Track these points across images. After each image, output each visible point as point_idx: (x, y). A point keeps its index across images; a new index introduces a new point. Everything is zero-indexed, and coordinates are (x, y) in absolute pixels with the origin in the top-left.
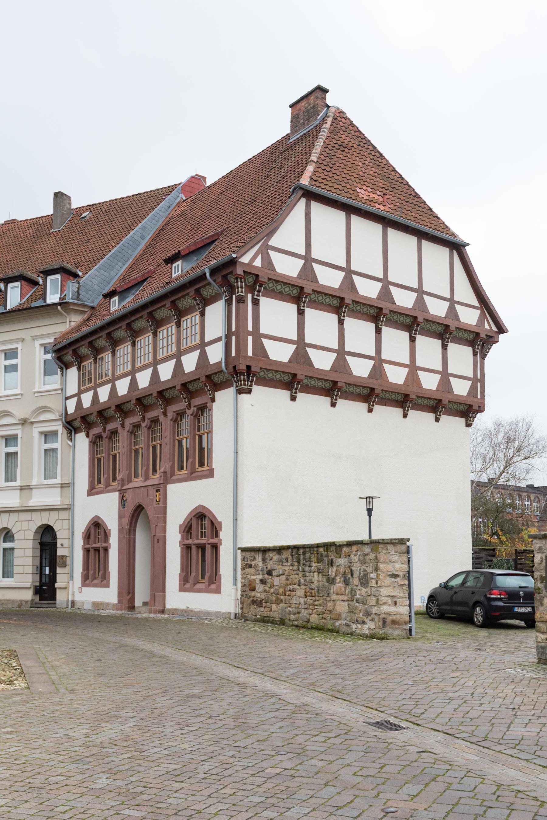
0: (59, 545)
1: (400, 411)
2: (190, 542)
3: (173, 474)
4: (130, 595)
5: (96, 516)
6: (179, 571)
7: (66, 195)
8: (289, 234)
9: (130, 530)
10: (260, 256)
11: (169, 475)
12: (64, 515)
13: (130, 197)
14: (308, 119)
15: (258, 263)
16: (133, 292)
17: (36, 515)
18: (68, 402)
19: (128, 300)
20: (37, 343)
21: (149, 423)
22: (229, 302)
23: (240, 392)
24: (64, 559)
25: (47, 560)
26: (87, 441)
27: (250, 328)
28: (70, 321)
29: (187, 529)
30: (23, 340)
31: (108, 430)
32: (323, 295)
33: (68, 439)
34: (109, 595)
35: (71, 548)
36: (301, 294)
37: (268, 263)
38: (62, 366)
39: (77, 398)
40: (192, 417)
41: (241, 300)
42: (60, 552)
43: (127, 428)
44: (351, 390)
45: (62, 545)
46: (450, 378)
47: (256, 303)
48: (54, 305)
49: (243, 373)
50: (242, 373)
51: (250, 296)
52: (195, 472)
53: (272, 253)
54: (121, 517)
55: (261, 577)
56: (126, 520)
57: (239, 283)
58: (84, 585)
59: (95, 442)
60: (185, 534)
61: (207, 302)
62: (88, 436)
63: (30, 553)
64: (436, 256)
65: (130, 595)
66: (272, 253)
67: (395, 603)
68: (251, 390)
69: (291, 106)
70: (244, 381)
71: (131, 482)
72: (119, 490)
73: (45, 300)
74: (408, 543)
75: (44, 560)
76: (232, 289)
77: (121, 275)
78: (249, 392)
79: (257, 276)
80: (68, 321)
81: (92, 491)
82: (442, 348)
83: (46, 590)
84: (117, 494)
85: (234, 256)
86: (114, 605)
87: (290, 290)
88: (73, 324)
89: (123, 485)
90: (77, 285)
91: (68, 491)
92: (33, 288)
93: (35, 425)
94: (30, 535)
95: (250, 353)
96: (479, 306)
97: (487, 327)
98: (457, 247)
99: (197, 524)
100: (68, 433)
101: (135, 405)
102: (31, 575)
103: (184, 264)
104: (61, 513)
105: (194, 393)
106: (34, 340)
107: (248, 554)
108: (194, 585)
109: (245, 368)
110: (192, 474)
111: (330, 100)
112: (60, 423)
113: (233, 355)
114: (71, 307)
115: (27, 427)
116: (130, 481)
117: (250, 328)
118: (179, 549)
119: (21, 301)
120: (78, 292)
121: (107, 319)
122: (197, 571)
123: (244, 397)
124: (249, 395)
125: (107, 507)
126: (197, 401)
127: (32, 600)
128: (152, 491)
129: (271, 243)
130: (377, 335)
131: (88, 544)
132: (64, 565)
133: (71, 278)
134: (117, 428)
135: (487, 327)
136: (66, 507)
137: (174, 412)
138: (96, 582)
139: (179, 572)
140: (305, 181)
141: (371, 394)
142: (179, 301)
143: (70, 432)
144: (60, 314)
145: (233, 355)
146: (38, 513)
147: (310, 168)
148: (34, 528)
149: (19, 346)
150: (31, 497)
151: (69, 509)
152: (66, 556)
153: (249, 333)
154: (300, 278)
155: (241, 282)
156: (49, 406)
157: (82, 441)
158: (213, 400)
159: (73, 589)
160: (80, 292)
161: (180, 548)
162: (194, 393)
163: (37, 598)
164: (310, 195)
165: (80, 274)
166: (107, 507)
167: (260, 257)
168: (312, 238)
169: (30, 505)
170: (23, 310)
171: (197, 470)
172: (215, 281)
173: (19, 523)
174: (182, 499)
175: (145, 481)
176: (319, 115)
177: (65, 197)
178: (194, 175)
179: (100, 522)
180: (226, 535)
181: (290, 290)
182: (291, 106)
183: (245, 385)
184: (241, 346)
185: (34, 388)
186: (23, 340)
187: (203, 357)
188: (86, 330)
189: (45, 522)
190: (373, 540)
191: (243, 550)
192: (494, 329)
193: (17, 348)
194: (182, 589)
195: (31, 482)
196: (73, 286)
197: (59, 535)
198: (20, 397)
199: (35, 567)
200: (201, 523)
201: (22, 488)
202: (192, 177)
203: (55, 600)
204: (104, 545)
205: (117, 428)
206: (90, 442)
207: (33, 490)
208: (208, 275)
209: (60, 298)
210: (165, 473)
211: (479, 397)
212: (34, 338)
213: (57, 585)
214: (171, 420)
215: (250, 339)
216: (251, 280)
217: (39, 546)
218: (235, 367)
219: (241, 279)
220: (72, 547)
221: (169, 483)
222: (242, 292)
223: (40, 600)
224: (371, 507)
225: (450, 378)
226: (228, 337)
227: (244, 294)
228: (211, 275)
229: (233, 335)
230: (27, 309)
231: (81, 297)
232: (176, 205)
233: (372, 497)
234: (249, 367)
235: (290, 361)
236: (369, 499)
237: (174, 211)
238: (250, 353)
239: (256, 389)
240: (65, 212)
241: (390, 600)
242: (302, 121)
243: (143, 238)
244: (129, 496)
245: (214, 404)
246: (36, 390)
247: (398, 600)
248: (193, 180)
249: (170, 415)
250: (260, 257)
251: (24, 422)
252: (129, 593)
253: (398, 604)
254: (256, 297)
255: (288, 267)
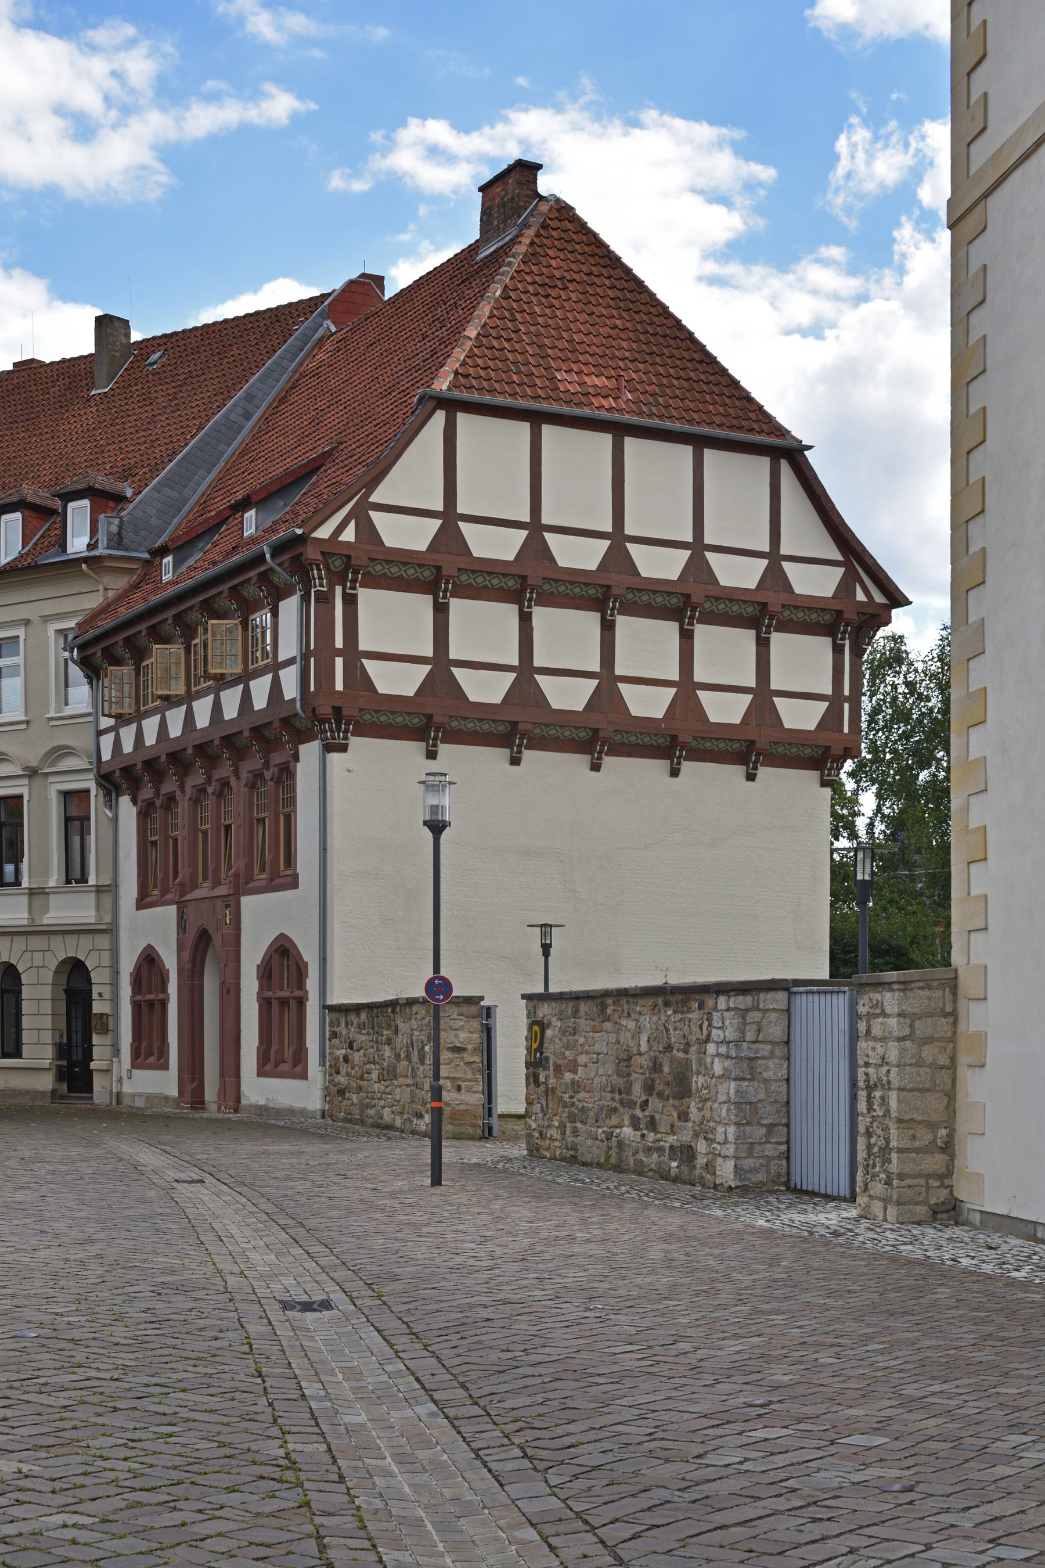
0: (95, 996)
1: (664, 765)
2: (269, 994)
3: (250, 878)
4: (196, 1083)
5: (282, 934)
6: (256, 1043)
7: (119, 318)
8: (414, 477)
9: (193, 971)
10: (353, 523)
11: (242, 880)
12: (103, 942)
13: (240, 318)
14: (505, 221)
15: (349, 535)
16: (200, 546)
17: (56, 942)
18: (103, 738)
19: (191, 562)
20: (53, 627)
21: (218, 788)
22: (305, 599)
23: (328, 748)
24: (104, 1019)
25: (79, 1020)
26: (134, 810)
27: (339, 643)
28: (106, 589)
29: (266, 973)
30: (27, 622)
31: (143, 801)
32: (485, 575)
33: (105, 805)
34: (164, 1082)
35: (115, 1000)
36: (443, 574)
37: (368, 532)
38: (90, 674)
39: (113, 733)
40: (272, 783)
41: (325, 600)
42: (97, 1008)
43: (188, 794)
44: (551, 733)
45: (100, 995)
46: (775, 699)
47: (350, 601)
48: (77, 561)
49: (342, 714)
50: (323, 721)
51: (338, 590)
52: (279, 877)
53: (374, 515)
54: (180, 948)
55: (343, 1052)
56: (186, 955)
57: (315, 572)
58: (134, 1066)
59: (144, 815)
60: (265, 980)
61: (279, 594)
62: (134, 801)
63: (47, 1007)
64: (738, 487)
65: (196, 1083)
66: (374, 515)
67: (459, 1088)
68: (347, 745)
69: (481, 189)
70: (331, 731)
71: (197, 888)
72: (177, 903)
73: (63, 547)
74: (482, 1003)
75: (74, 1021)
76: (307, 584)
77: (204, 494)
78: (343, 748)
79: (349, 557)
80: (101, 588)
81: (142, 903)
82: (758, 644)
83: (75, 1072)
84: (174, 907)
85: (299, 531)
86: (174, 1099)
87: (417, 572)
88: (111, 594)
89: (183, 893)
90: (117, 521)
91: (107, 900)
92: (47, 521)
93: (51, 779)
94: (48, 976)
95: (339, 686)
96: (841, 558)
97: (861, 596)
98: (786, 453)
99: (281, 965)
100: (105, 796)
101: (195, 754)
102: (50, 1047)
103: (261, 515)
104: (97, 937)
105: (268, 744)
106: (45, 622)
107: (336, 1015)
108: (277, 1065)
109: (330, 711)
110: (272, 880)
111: (545, 184)
112: (91, 776)
113: (312, 689)
114: (106, 564)
115: (38, 782)
116: (195, 886)
117: (339, 643)
118: (256, 1005)
119: (23, 548)
120: (119, 533)
121: (155, 599)
122: (282, 1042)
123: (334, 758)
124: (343, 754)
125: (156, 929)
126: (277, 758)
127: (54, 1092)
128: (219, 903)
129: (374, 498)
130: (606, 632)
131: (140, 994)
132: (104, 1030)
133: (111, 504)
134: (175, 792)
135: (861, 596)
136: (104, 927)
137: (250, 772)
138: (151, 1060)
139: (257, 1044)
140: (442, 384)
141: (601, 734)
142: (242, 589)
143: (108, 794)
144: (85, 575)
145: (312, 689)
146: (60, 938)
147: (459, 354)
148: (53, 965)
149: (21, 632)
150: (46, 909)
151: (111, 931)
152: (107, 1015)
153: (339, 653)
154: (432, 552)
155: (319, 569)
156: (71, 744)
157: (127, 810)
158: (296, 758)
159: (123, 1075)
160: (124, 534)
161: (257, 1005)
162: (268, 744)
163: (64, 1087)
164: (452, 406)
165: (129, 493)
166: (156, 929)
167: (352, 524)
168: (473, 474)
169: (45, 922)
170: (23, 568)
171: (282, 874)
172: (280, 565)
173: (27, 955)
174: (263, 919)
175: (213, 888)
176: (519, 217)
177: (117, 324)
178: (354, 275)
179: (288, 947)
180: (312, 984)
181: (417, 572)
182: (481, 189)
183: (334, 738)
184: (326, 674)
185: (48, 713)
186: (27, 622)
187: (276, 687)
188: (124, 613)
189: (71, 954)
190: (553, 994)
191: (333, 1009)
192: (879, 598)
193: (18, 637)
194: (261, 1073)
195: (47, 881)
196: (109, 524)
197: (94, 977)
198: (24, 726)
199: (58, 1033)
200: (283, 959)
201: (32, 893)
202: (351, 282)
203: (91, 1091)
204: (161, 996)
205: (175, 792)
206: (139, 813)
207: (51, 896)
208: (268, 556)
209: (89, 545)
210: (236, 876)
211: (846, 730)
212: (47, 619)
213: (93, 1065)
214: (246, 785)
215: (339, 662)
216: (338, 563)
217: (64, 997)
218: (314, 709)
219: (318, 566)
220: (116, 1001)
221: (245, 894)
222: (321, 585)
223: (69, 1091)
224: (548, 942)
225: (775, 699)
226: (305, 656)
227: (325, 589)
228: (273, 557)
229: (316, 654)
230: (30, 567)
231: (125, 542)
232: (316, 345)
233: (551, 926)
234: (337, 710)
235: (419, 692)
236: (546, 928)
237: (311, 357)
238: (339, 686)
239: (354, 742)
240: (118, 354)
241: (449, 1084)
242: (496, 222)
243: (248, 416)
244: (190, 911)
245: (298, 765)
246: (52, 714)
247: (463, 1085)
248: (354, 288)
249: (244, 776)
250: (352, 524)
251: (32, 773)
252: (193, 1080)
253: (463, 1090)
254: (348, 591)
255: (407, 535)
